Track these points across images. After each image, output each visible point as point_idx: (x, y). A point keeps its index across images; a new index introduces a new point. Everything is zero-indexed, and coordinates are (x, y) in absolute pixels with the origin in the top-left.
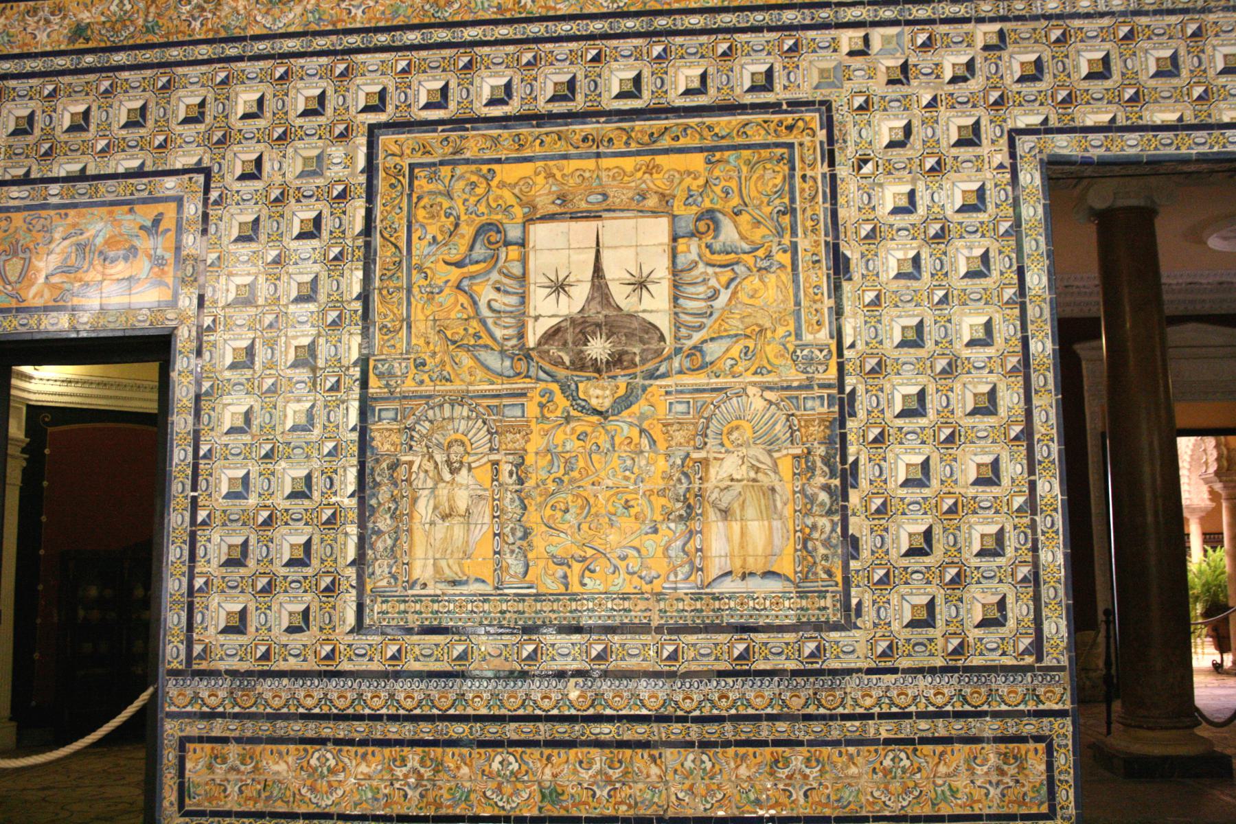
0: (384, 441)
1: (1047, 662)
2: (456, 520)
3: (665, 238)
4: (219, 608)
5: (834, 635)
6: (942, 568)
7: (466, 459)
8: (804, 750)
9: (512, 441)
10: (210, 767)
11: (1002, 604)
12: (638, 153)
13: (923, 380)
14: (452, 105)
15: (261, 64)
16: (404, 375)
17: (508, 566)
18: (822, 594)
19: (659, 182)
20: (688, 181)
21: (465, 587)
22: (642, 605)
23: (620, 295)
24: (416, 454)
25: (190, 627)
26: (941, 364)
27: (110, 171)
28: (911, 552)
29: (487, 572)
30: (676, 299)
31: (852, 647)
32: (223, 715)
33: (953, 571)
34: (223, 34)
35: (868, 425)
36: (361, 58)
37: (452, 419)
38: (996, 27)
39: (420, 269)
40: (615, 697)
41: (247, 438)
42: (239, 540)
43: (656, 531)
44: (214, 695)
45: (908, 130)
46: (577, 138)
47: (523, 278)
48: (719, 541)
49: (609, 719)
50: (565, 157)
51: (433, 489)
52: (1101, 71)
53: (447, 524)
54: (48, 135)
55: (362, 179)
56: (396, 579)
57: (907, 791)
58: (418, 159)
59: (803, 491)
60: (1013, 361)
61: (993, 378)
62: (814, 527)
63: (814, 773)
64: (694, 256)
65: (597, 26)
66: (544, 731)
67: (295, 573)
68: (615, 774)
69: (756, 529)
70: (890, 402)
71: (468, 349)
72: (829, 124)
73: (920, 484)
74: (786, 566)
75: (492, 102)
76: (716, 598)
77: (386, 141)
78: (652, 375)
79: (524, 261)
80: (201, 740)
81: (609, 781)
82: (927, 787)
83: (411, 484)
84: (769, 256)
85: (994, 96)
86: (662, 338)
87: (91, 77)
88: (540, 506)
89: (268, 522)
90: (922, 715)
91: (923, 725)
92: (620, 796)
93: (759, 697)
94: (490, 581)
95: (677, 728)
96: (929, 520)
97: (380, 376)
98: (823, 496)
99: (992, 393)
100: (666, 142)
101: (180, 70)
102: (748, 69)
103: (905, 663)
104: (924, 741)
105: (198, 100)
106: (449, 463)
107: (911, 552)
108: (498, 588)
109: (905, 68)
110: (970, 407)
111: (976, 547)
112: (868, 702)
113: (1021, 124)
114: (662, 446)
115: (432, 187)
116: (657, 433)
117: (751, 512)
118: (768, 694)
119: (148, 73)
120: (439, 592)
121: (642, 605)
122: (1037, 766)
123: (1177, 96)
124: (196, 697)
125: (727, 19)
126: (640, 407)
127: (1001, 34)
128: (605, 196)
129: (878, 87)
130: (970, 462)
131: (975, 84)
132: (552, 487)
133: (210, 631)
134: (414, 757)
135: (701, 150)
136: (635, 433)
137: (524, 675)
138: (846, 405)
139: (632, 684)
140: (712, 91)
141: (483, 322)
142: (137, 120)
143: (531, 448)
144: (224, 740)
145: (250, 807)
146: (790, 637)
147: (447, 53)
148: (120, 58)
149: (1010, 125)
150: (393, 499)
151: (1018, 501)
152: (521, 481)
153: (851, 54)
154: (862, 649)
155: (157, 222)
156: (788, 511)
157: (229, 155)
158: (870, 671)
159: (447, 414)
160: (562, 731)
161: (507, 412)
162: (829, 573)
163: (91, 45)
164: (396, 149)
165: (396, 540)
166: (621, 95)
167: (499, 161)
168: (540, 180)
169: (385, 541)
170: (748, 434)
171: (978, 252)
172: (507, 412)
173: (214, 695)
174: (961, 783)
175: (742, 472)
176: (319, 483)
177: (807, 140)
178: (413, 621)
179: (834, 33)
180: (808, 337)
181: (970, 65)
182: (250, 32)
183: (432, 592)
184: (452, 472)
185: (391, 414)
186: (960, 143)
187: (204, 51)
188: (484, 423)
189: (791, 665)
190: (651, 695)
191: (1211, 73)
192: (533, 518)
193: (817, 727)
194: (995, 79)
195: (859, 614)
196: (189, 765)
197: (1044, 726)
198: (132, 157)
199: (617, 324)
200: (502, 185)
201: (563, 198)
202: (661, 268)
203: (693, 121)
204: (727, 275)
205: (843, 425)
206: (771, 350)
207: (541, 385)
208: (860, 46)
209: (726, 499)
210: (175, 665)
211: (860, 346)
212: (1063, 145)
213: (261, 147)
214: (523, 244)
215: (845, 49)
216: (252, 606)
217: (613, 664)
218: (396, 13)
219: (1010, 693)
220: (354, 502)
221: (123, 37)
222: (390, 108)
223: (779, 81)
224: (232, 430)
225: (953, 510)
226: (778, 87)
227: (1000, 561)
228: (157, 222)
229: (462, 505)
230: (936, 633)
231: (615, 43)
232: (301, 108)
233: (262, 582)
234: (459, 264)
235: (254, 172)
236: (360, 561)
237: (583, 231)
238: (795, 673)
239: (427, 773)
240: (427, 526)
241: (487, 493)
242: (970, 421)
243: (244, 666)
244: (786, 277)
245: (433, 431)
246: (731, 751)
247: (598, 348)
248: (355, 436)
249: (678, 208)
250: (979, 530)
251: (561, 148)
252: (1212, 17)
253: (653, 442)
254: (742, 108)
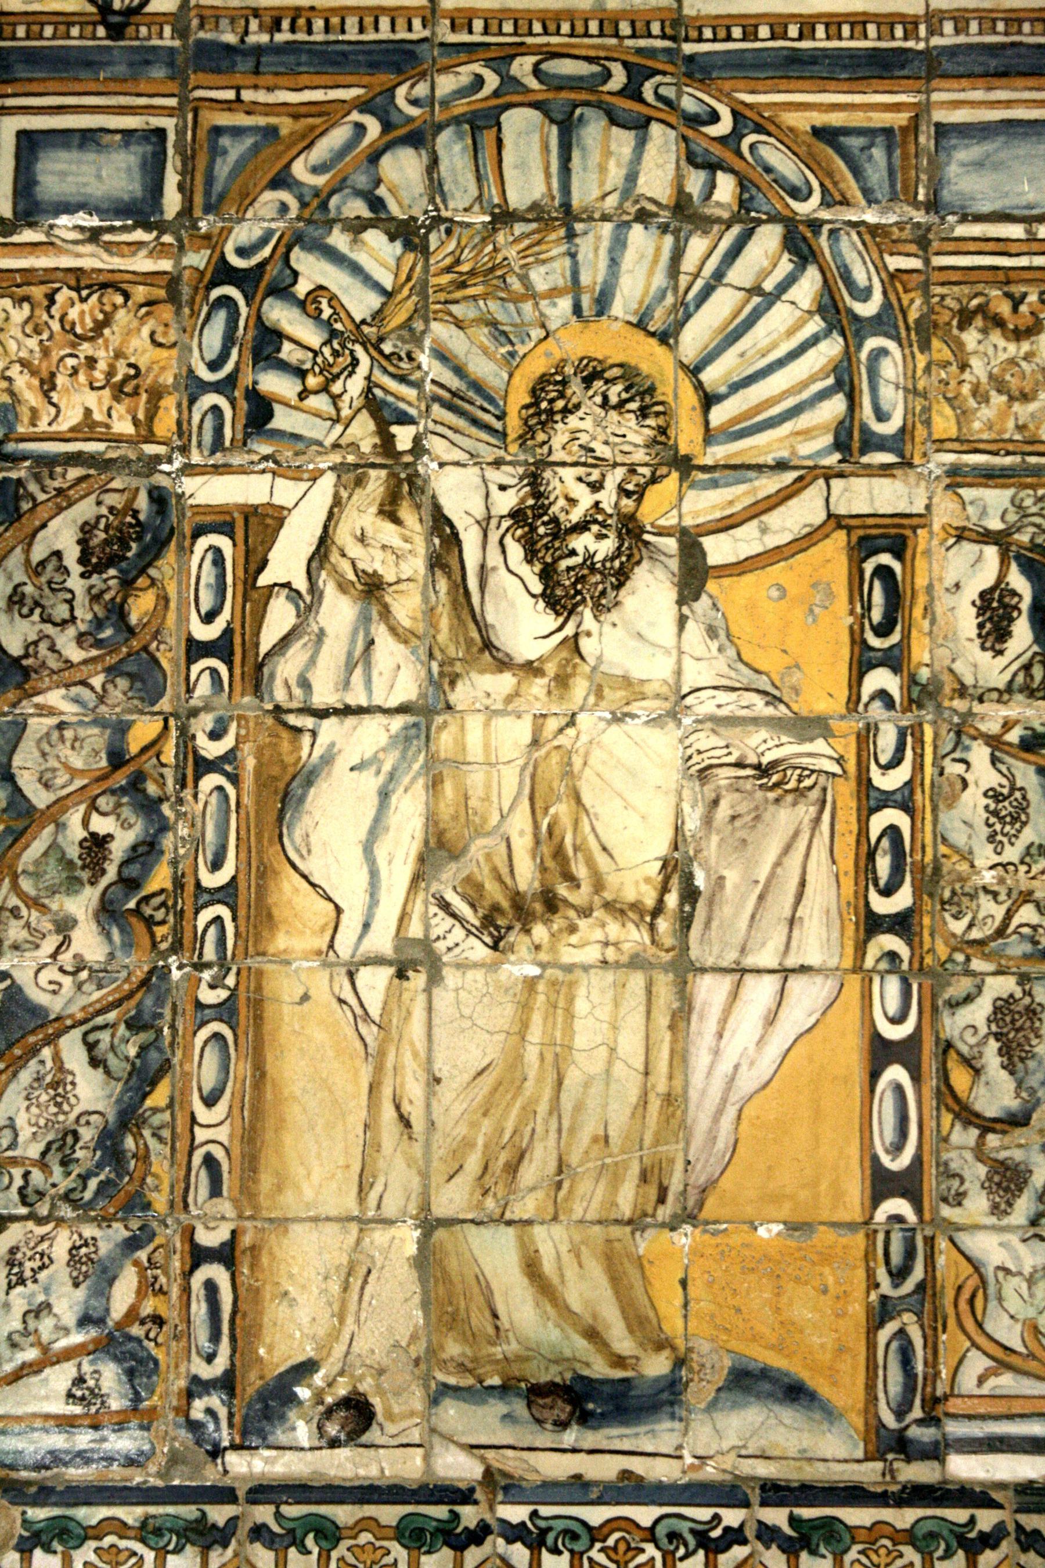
2: (586, 943)
7: (664, 506)
17: (980, 1285)
21: (662, 1434)
24: (292, 460)
29: (819, 1325)
37: (563, 217)
51: (423, 715)
53: (520, 967)
56: (139, 1368)
83: (256, 677)
94: (844, 1391)
106: (536, 527)
108: (901, 1446)
120: (458, 1467)
150: (125, 776)
159: (526, 183)
161: (966, 177)
165: (144, 1077)
169: (59, 1083)
172: (966, 177)
183: (408, 1467)
184: (559, 598)
185: (115, 174)
188: (800, 245)
240: (374, 983)
241: (820, 753)
245: (421, 300)
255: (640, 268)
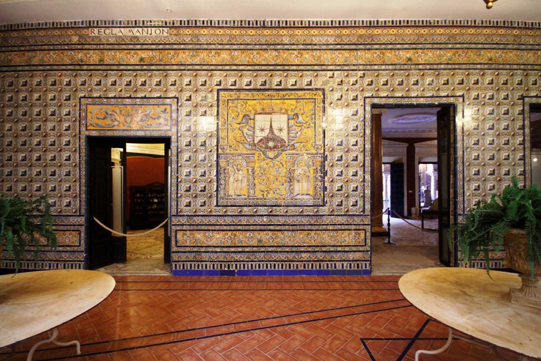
0: (222, 163)
1: (366, 214)
2: (239, 182)
3: (286, 119)
4: (184, 201)
5: (321, 208)
6: (344, 194)
8: (314, 232)
9: (251, 164)
10: (183, 236)
11: (357, 202)
12: (280, 99)
13: (342, 153)
14: (237, 85)
15: (190, 72)
16: (227, 149)
18: (319, 199)
19: (285, 106)
20: (292, 106)
22: (280, 201)
23: (276, 132)
25: (177, 205)
26: (346, 150)
27: (152, 96)
28: (338, 190)
30: (288, 133)
31: (325, 210)
32: (185, 225)
33: (347, 194)
34: (180, 63)
35: (330, 163)
36: (215, 72)
38: (363, 72)
39: (230, 124)
40: (275, 220)
41: (190, 162)
42: (189, 186)
43: (283, 185)
44: (183, 220)
45: (341, 96)
46: (267, 95)
47: (254, 128)
48: (297, 188)
49: (273, 225)
50: (264, 99)
52: (386, 84)
54: (135, 86)
55: (216, 102)
57: (335, 240)
58: (229, 98)
59: (315, 177)
60: (362, 149)
61: (357, 153)
62: (317, 185)
63: (316, 236)
64: (293, 124)
65: (271, 68)
66: (258, 228)
67: (202, 193)
68: (274, 237)
69: (305, 185)
70: (335, 158)
71: (242, 143)
72: (324, 94)
73: (341, 176)
74: (311, 193)
75: (247, 85)
76: (296, 199)
77: (221, 93)
78: (283, 151)
79: (254, 124)
80: (180, 230)
81: (272, 238)
82: (340, 240)
84: (309, 124)
85: (361, 89)
86: (285, 142)
87: (146, 72)
88: (258, 179)
89: (195, 182)
90: (339, 225)
91: (339, 227)
92: (275, 241)
93: (305, 220)
95: (287, 227)
96: (342, 183)
97: (221, 149)
98: (320, 178)
99: (357, 157)
100: (287, 97)
101: (169, 72)
102: (306, 80)
103: (336, 214)
104: (339, 230)
105: (174, 80)
106: (237, 169)
107: (338, 190)
109: (342, 81)
110: (352, 159)
111: (352, 189)
112: (328, 222)
113: (367, 96)
114: (285, 166)
115: (233, 105)
116: (284, 164)
117: (304, 181)
118: (307, 220)
119: (161, 72)
121: (280, 201)
122: (363, 235)
123: (402, 90)
124: (179, 221)
125: (302, 68)
126: (280, 157)
127: (364, 74)
128: (273, 109)
129: (335, 86)
130: (351, 171)
131: (357, 86)
132: (260, 175)
133: (182, 206)
134: (230, 233)
135: (295, 99)
136: (279, 163)
137: (254, 216)
138: (325, 158)
139: (278, 217)
140: (298, 85)
141: (245, 137)
142: (159, 84)
143: (256, 166)
144: (186, 230)
145: (192, 245)
146: (312, 208)
147: (236, 72)
148: (153, 67)
149: (364, 96)
151: (361, 180)
152: (253, 173)
153: (330, 77)
154: (327, 210)
155: (165, 110)
156: (312, 181)
157: (183, 94)
158: (328, 215)
160: (262, 227)
162: (320, 194)
163: (145, 63)
164: (224, 95)
166: (277, 85)
167: (248, 100)
168: (258, 104)
170: (304, 164)
171: (356, 125)
173: (183, 220)
174: (347, 239)
175: (302, 172)
176: (207, 173)
177: (319, 98)
178: (229, 204)
179: (326, 72)
180: (317, 143)
181: (356, 81)
182: (187, 63)
186: (353, 100)
187: (175, 67)
189: (312, 214)
190: (282, 220)
191: (410, 85)
192: (256, 182)
193: (317, 227)
194: (362, 85)
195: (326, 203)
196: (178, 236)
197: (365, 227)
198: (158, 93)
199: (274, 139)
200: (249, 105)
201: (263, 109)
202: (285, 126)
203: (293, 92)
204: (300, 128)
205: (324, 162)
206: (309, 146)
207: (258, 152)
208: (332, 75)
209: (299, 178)
210: (174, 214)
211: (329, 145)
212: (376, 101)
213: (191, 93)
214: (254, 120)
215: (328, 76)
216: (192, 201)
217: (274, 213)
218: (223, 61)
219: (357, 220)
220: (215, 178)
221: (154, 62)
222: (222, 85)
223: (313, 83)
224: (186, 161)
225: (347, 181)
226: (313, 84)
227: (357, 192)
228: (165, 110)
229: (240, 178)
230: (343, 207)
231: (275, 72)
232: (200, 84)
233: (194, 195)
234: (239, 124)
235: (189, 99)
236: (217, 191)
237: (268, 117)
238: (313, 215)
239: (233, 237)
242: (352, 162)
243: (190, 214)
244: (313, 129)
246: (299, 232)
247: (271, 144)
248: (216, 162)
249: (289, 113)
250: (352, 186)
251: (263, 97)
252: (412, 71)
253: (283, 165)
254: (304, 90)
255: (240, 161)
